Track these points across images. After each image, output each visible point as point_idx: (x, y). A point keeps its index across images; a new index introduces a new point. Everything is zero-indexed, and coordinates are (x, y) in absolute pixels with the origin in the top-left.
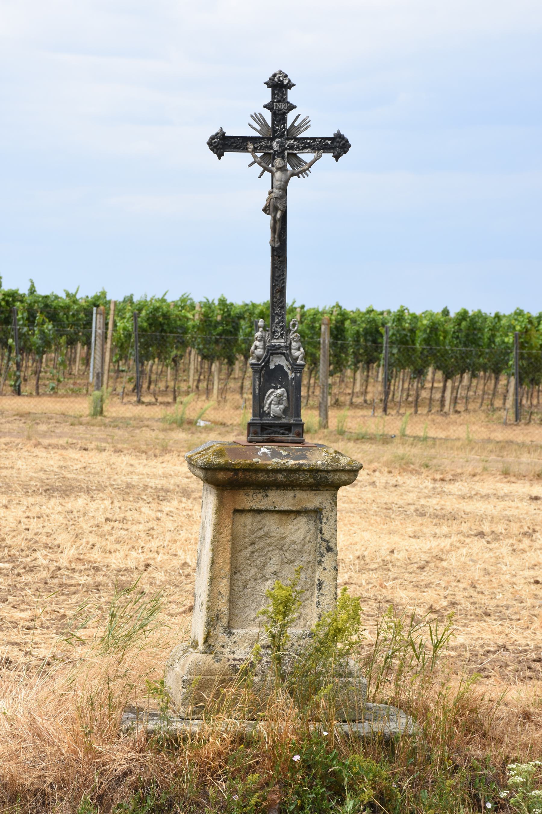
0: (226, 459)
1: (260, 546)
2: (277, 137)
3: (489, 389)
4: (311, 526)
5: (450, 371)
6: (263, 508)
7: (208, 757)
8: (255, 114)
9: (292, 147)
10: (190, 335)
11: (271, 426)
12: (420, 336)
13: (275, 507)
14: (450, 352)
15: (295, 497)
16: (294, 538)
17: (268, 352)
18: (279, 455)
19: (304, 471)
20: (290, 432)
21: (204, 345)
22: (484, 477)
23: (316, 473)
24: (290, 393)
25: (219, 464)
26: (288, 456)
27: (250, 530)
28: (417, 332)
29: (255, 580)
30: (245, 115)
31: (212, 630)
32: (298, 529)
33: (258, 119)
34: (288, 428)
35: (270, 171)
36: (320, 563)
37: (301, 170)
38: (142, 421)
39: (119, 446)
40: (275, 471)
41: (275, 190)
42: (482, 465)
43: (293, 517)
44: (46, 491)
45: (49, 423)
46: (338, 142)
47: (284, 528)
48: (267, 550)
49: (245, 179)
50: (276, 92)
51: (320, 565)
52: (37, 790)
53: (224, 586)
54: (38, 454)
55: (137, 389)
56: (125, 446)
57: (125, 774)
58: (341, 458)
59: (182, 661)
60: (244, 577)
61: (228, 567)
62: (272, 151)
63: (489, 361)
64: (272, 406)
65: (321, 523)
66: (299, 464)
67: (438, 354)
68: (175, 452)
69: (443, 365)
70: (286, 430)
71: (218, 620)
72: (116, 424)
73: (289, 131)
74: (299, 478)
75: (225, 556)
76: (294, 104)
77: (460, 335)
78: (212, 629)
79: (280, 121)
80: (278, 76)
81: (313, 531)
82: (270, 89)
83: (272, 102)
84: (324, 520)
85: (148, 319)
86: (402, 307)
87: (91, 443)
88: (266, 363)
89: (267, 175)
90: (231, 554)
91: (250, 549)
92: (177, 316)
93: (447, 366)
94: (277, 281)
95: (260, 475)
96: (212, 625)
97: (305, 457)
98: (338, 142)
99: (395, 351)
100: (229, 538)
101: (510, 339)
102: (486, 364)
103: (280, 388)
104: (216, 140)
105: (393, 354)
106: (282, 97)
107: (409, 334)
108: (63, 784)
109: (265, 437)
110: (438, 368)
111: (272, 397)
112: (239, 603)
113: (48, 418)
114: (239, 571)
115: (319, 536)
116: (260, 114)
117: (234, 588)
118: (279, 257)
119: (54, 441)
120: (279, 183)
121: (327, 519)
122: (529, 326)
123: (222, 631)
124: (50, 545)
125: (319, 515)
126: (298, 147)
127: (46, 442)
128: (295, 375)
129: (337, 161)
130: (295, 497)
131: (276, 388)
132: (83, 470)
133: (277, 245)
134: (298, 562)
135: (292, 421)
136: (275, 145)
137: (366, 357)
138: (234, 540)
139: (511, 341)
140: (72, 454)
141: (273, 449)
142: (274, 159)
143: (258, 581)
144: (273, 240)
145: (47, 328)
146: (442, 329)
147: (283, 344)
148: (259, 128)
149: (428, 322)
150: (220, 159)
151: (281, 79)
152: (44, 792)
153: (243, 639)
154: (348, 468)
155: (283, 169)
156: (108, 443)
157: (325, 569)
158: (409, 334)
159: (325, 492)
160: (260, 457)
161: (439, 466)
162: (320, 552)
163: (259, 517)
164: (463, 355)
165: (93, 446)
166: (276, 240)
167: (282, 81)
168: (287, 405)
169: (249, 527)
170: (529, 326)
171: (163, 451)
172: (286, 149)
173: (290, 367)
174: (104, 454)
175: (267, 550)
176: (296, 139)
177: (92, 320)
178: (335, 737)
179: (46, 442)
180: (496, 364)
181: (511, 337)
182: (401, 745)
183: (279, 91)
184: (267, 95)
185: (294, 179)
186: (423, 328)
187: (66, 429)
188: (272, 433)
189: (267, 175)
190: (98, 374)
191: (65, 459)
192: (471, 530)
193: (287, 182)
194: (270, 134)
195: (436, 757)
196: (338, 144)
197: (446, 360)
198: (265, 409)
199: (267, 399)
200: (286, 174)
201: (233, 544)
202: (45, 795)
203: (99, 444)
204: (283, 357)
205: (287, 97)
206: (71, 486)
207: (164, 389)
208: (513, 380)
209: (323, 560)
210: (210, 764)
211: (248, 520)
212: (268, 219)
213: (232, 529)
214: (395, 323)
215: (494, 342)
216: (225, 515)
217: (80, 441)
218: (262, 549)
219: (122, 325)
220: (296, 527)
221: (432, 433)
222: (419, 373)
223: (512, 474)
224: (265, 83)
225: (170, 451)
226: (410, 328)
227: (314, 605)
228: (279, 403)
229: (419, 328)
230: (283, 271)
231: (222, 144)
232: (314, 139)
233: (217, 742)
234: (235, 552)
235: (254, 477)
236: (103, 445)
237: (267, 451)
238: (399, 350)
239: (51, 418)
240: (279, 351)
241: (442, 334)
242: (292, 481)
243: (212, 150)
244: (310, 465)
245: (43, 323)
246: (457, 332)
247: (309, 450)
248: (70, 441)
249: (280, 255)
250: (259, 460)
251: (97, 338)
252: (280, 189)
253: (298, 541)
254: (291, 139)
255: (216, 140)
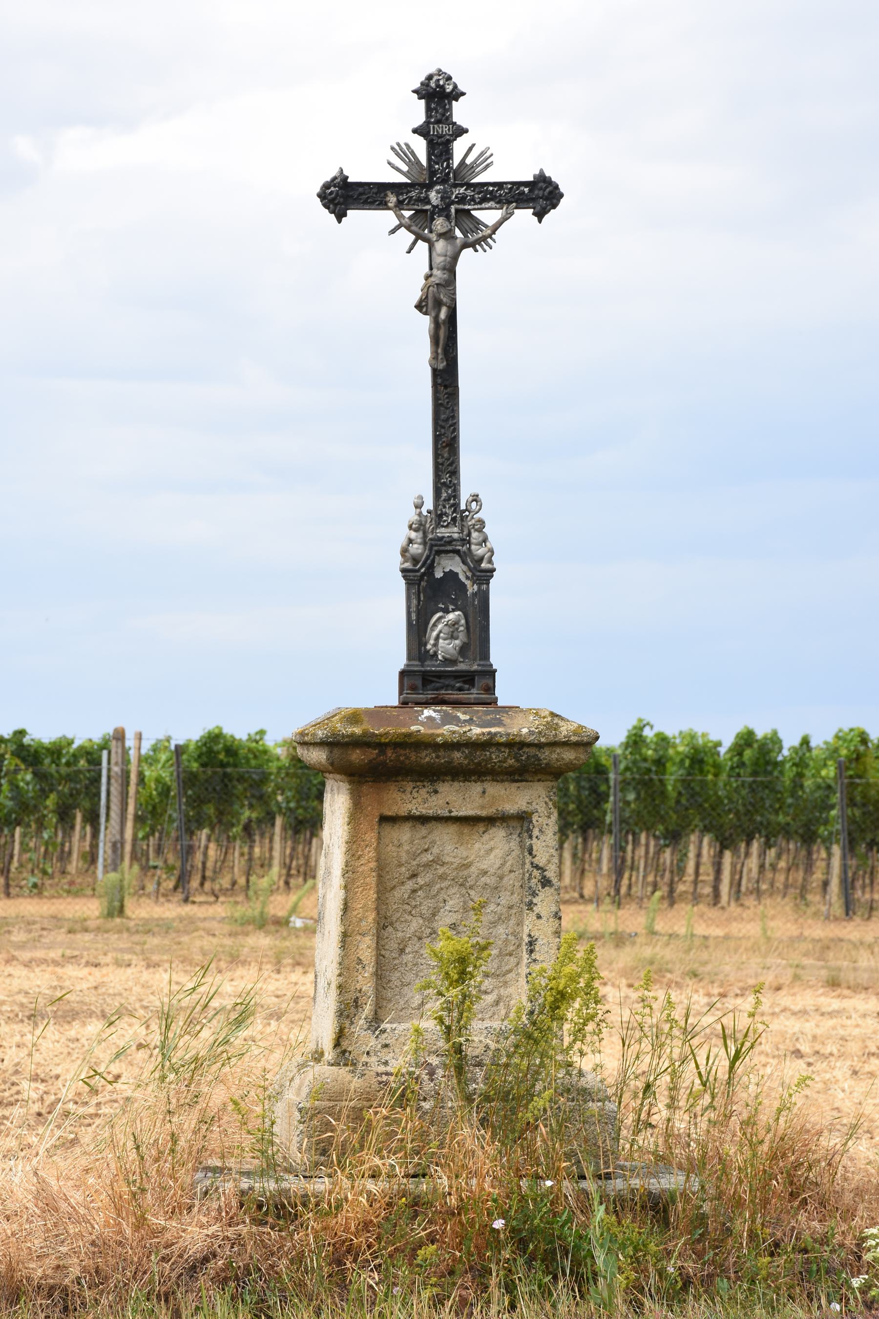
0: (364, 727)
1: (427, 880)
2: (436, 183)
3: (796, 881)
4: (514, 844)
5: (727, 834)
6: (431, 812)
7: (347, 1229)
8: (398, 144)
9: (462, 200)
10: (272, 784)
11: (440, 675)
12: (673, 776)
13: (450, 812)
14: (726, 801)
15: (484, 792)
16: (484, 866)
17: (431, 550)
18: (457, 721)
19: (499, 745)
20: (473, 686)
21: (298, 802)
22: (796, 990)
23: (520, 749)
24: (470, 619)
25: (353, 735)
26: (470, 721)
27: (408, 852)
28: (668, 765)
29: (420, 939)
30: (381, 142)
31: (347, 1025)
32: (491, 849)
33: (404, 152)
34: (469, 679)
35: (426, 240)
36: (530, 905)
37: (479, 238)
38: (193, 923)
39: (155, 958)
40: (451, 746)
41: (435, 272)
42: (790, 972)
43: (482, 829)
44: (29, 1018)
45: (30, 931)
46: (541, 189)
47: (467, 849)
48: (438, 886)
49: (386, 254)
50: (433, 106)
51: (531, 909)
52: (52, 1288)
53: (365, 948)
54: (12, 972)
55: (182, 881)
56: (165, 958)
57: (206, 1260)
58: (561, 723)
59: (297, 1081)
60: (400, 934)
61: (371, 916)
62: (428, 207)
63: (794, 820)
64: (441, 641)
65: (531, 837)
66: (489, 733)
67: (706, 805)
68: (253, 964)
69: (714, 823)
70: (465, 682)
71: (357, 1007)
72: (147, 928)
73: (456, 172)
74: (491, 758)
75: (367, 897)
76: (465, 126)
77: (742, 771)
78: (347, 1023)
79: (441, 155)
80: (435, 78)
81: (517, 852)
82: (423, 101)
83: (427, 123)
84: (536, 832)
85: (199, 756)
86: (640, 720)
87: (105, 954)
88: (427, 569)
89: (422, 247)
90: (378, 892)
91: (410, 885)
92: (250, 750)
93: (722, 826)
94: (443, 427)
95: (424, 754)
96: (348, 1016)
97: (500, 723)
98: (541, 189)
99: (631, 797)
100: (373, 865)
101: (829, 772)
102: (788, 824)
103: (454, 610)
104: (332, 189)
105: (628, 803)
106: (443, 115)
107: (654, 768)
108: (98, 1278)
109: (430, 695)
110: (706, 829)
111: (440, 626)
112: (393, 979)
113: (29, 924)
114: (391, 924)
115: (528, 859)
116: (407, 145)
117: (383, 952)
118: (446, 387)
119: (39, 954)
120: (442, 259)
121: (540, 831)
122: (862, 748)
123: (365, 1027)
124: (42, 1076)
125: (526, 824)
126: (473, 199)
127: (26, 955)
128: (479, 588)
129: (540, 221)
130: (484, 792)
131: (447, 612)
132: (93, 991)
133: (441, 366)
134: (492, 907)
135: (475, 667)
136: (434, 196)
137: (580, 817)
138: (381, 869)
139: (832, 774)
140: (71, 971)
141: (445, 712)
142: (433, 219)
143: (425, 940)
144: (435, 357)
145: (23, 780)
146: (711, 761)
147: (456, 536)
148: (405, 168)
149: (687, 749)
150: (339, 221)
151: (441, 83)
152: (65, 1290)
153: (402, 1039)
154: (574, 739)
155: (447, 236)
156: (135, 953)
157: (539, 917)
158: (654, 768)
159: (536, 784)
160: (422, 724)
161: (716, 974)
162: (530, 888)
163: (423, 830)
164: (750, 808)
165: (108, 959)
166: (440, 357)
167: (442, 87)
168: (465, 640)
169: (406, 847)
170: (862, 748)
171: (232, 962)
172: (453, 203)
173: (469, 574)
174: (129, 971)
175: (438, 886)
176: (469, 186)
177: (100, 776)
178: (566, 1197)
179: (26, 955)
180: (807, 825)
181: (832, 768)
182: (680, 1208)
183: (438, 104)
184: (418, 112)
185: (467, 253)
186: (678, 760)
187: (61, 936)
188: (442, 688)
189: (422, 246)
190: (114, 845)
191: (60, 978)
192: (778, 1049)
193: (455, 258)
194: (424, 178)
195: (742, 1226)
196: (541, 193)
197: (719, 815)
198: (429, 647)
199: (432, 630)
200: (453, 245)
201: (380, 876)
202: (67, 1295)
203: (119, 956)
204: (457, 558)
205: (451, 115)
206: (73, 1010)
207: (229, 887)
208: (836, 850)
209: (535, 901)
210: (352, 1240)
211: (404, 834)
212: (425, 321)
213: (377, 849)
214: (630, 750)
215: (802, 786)
216: (364, 827)
217: (85, 953)
218: (429, 885)
219: (154, 774)
220: (488, 847)
221: (700, 930)
222: (674, 837)
223: (844, 985)
224: (414, 92)
225: (244, 963)
226: (656, 757)
227: (522, 981)
228: (452, 637)
229: (671, 759)
230: (453, 411)
231: (342, 196)
232: (500, 185)
233: (360, 1199)
234: (383, 890)
235: (413, 758)
236: (127, 957)
237: (434, 715)
238: (638, 794)
239: (34, 923)
240: (449, 548)
241: (712, 770)
242: (479, 764)
243: (326, 206)
244: (508, 734)
245: (17, 771)
246: (738, 767)
247: (507, 713)
248: (68, 953)
249: (447, 383)
250: (421, 728)
251: (113, 781)
252: (444, 269)
253: (492, 871)
254: (462, 186)
255: (332, 189)
